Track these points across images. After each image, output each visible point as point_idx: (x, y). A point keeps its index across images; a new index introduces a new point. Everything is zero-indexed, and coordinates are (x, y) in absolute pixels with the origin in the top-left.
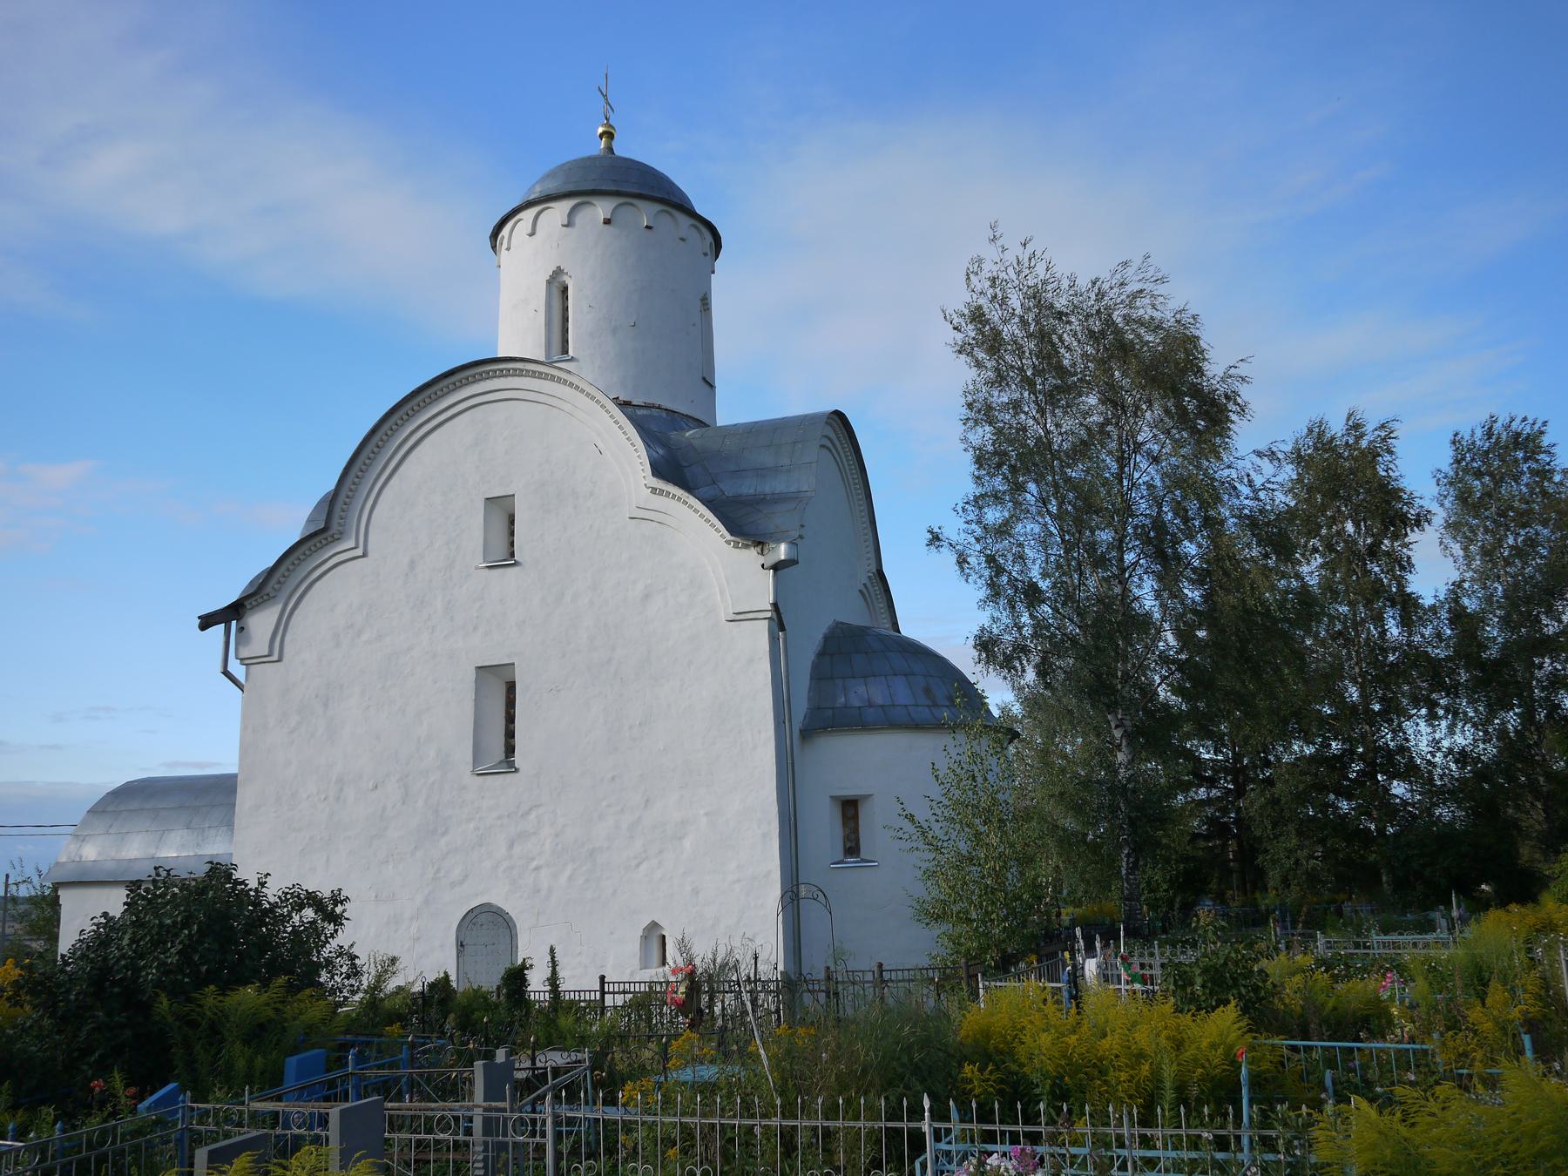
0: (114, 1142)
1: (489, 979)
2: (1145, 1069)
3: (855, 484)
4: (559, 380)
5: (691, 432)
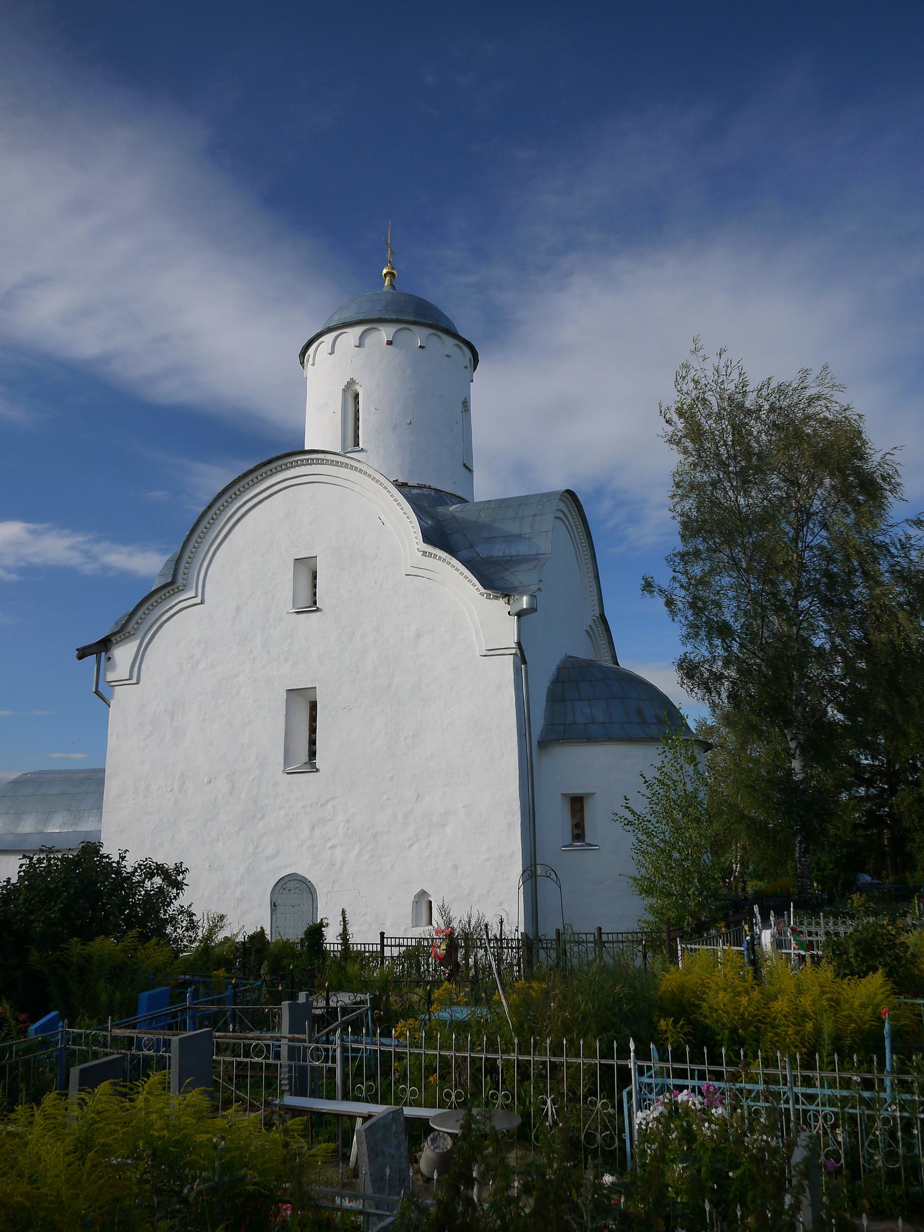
0: (11, 1057)
1: (295, 933)
2: (809, 1026)
3: (584, 551)
4: (352, 467)
5: (454, 507)
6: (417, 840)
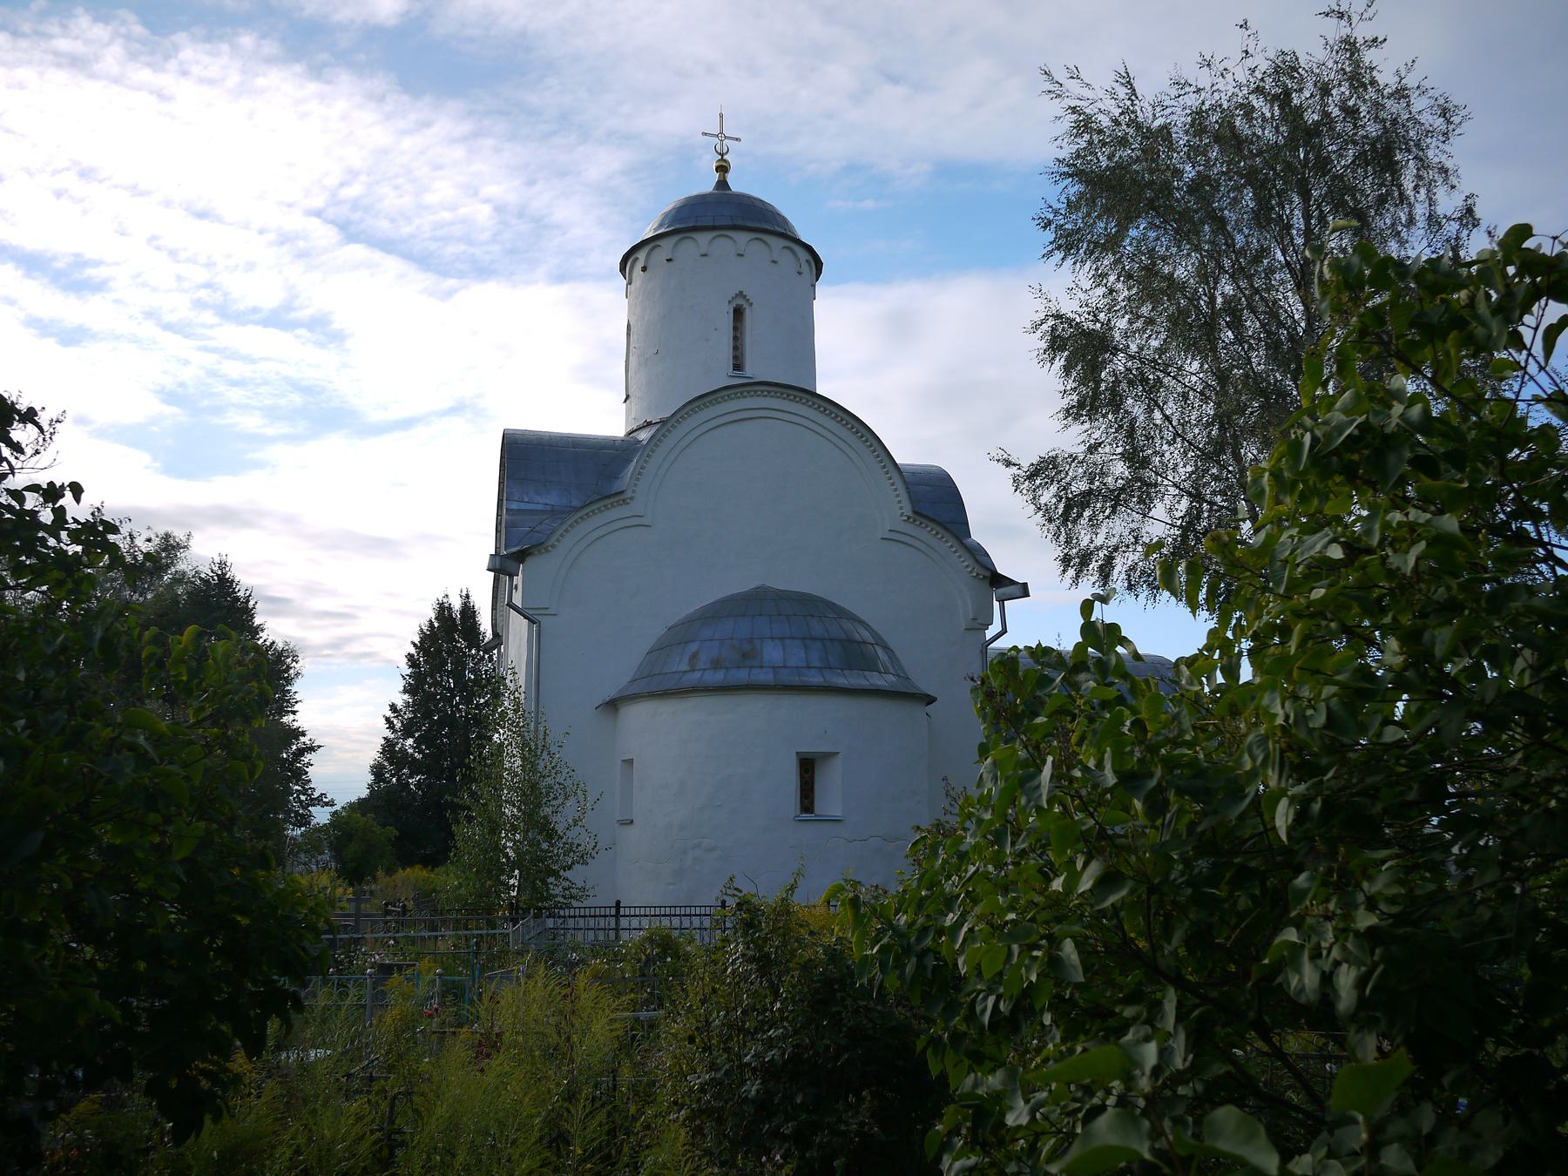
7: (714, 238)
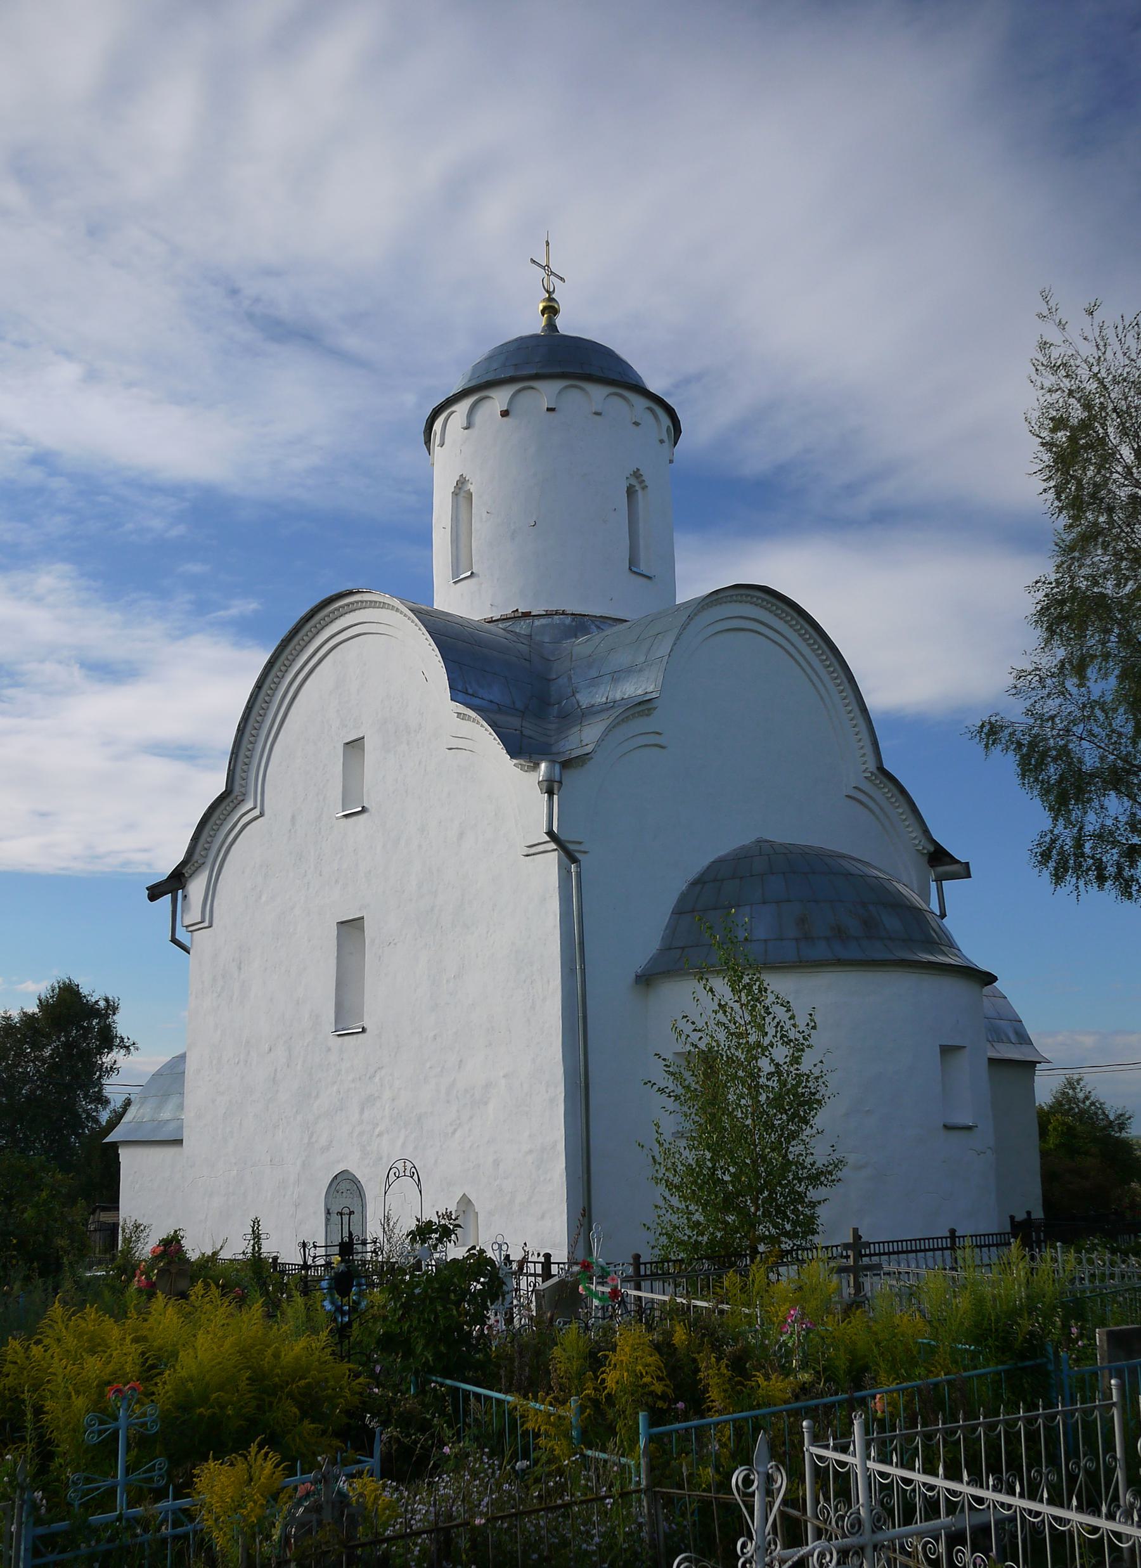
6: (460, 1124)
7: (519, 391)
